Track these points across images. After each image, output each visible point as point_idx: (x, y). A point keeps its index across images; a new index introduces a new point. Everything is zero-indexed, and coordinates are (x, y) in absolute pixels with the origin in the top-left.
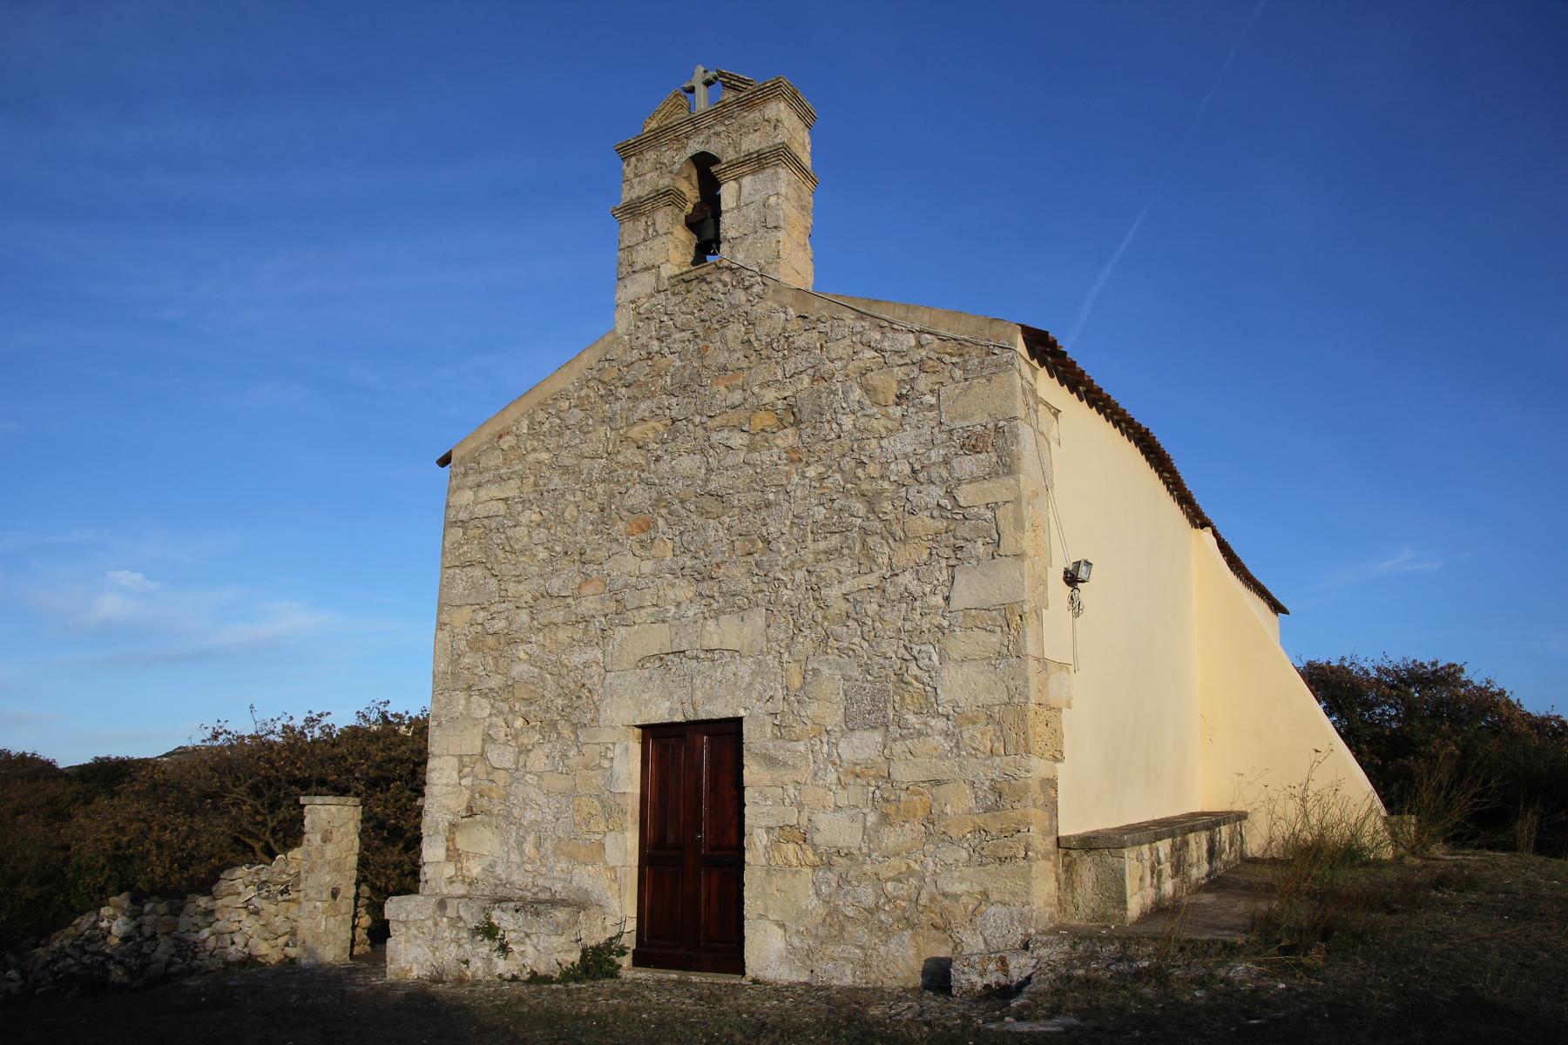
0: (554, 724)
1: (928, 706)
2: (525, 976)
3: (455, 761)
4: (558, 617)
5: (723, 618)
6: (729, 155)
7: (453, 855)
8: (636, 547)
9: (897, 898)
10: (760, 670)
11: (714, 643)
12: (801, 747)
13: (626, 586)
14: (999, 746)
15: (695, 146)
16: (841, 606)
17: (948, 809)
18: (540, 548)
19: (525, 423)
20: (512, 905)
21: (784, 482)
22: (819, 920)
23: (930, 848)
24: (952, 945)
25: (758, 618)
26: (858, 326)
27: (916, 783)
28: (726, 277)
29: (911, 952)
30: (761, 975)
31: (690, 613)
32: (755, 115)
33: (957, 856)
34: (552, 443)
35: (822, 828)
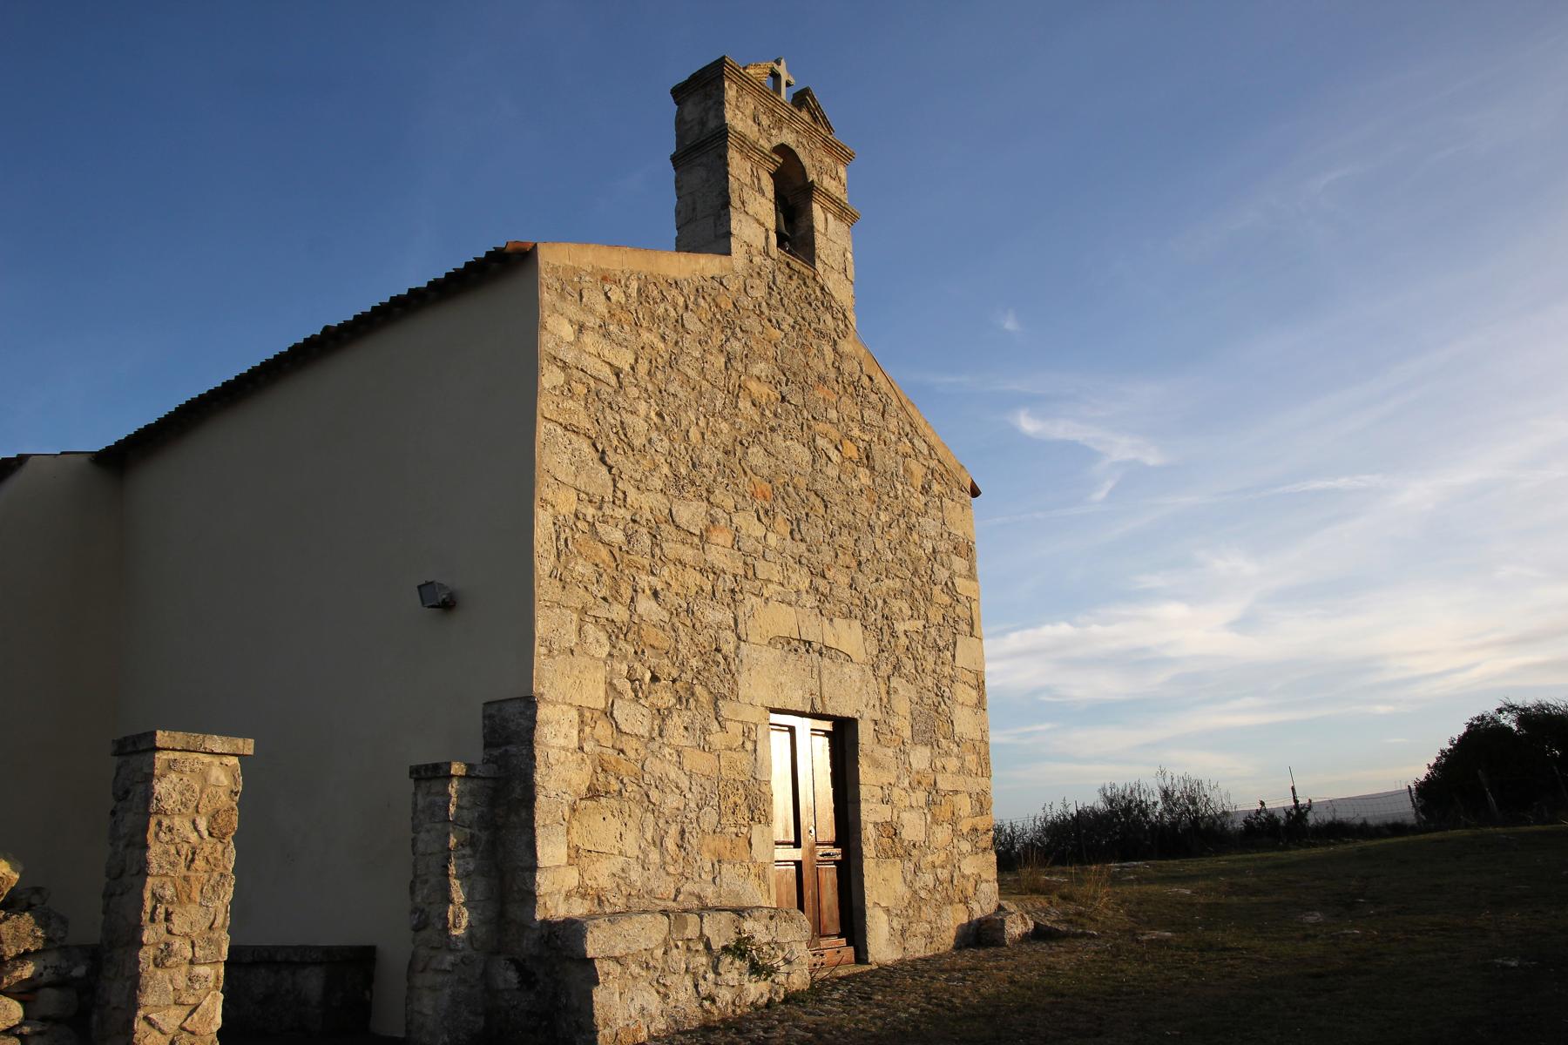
1: (951, 736)
3: (574, 714)
4: (689, 554)
12: (890, 752)
15: (788, 138)
19: (634, 285)
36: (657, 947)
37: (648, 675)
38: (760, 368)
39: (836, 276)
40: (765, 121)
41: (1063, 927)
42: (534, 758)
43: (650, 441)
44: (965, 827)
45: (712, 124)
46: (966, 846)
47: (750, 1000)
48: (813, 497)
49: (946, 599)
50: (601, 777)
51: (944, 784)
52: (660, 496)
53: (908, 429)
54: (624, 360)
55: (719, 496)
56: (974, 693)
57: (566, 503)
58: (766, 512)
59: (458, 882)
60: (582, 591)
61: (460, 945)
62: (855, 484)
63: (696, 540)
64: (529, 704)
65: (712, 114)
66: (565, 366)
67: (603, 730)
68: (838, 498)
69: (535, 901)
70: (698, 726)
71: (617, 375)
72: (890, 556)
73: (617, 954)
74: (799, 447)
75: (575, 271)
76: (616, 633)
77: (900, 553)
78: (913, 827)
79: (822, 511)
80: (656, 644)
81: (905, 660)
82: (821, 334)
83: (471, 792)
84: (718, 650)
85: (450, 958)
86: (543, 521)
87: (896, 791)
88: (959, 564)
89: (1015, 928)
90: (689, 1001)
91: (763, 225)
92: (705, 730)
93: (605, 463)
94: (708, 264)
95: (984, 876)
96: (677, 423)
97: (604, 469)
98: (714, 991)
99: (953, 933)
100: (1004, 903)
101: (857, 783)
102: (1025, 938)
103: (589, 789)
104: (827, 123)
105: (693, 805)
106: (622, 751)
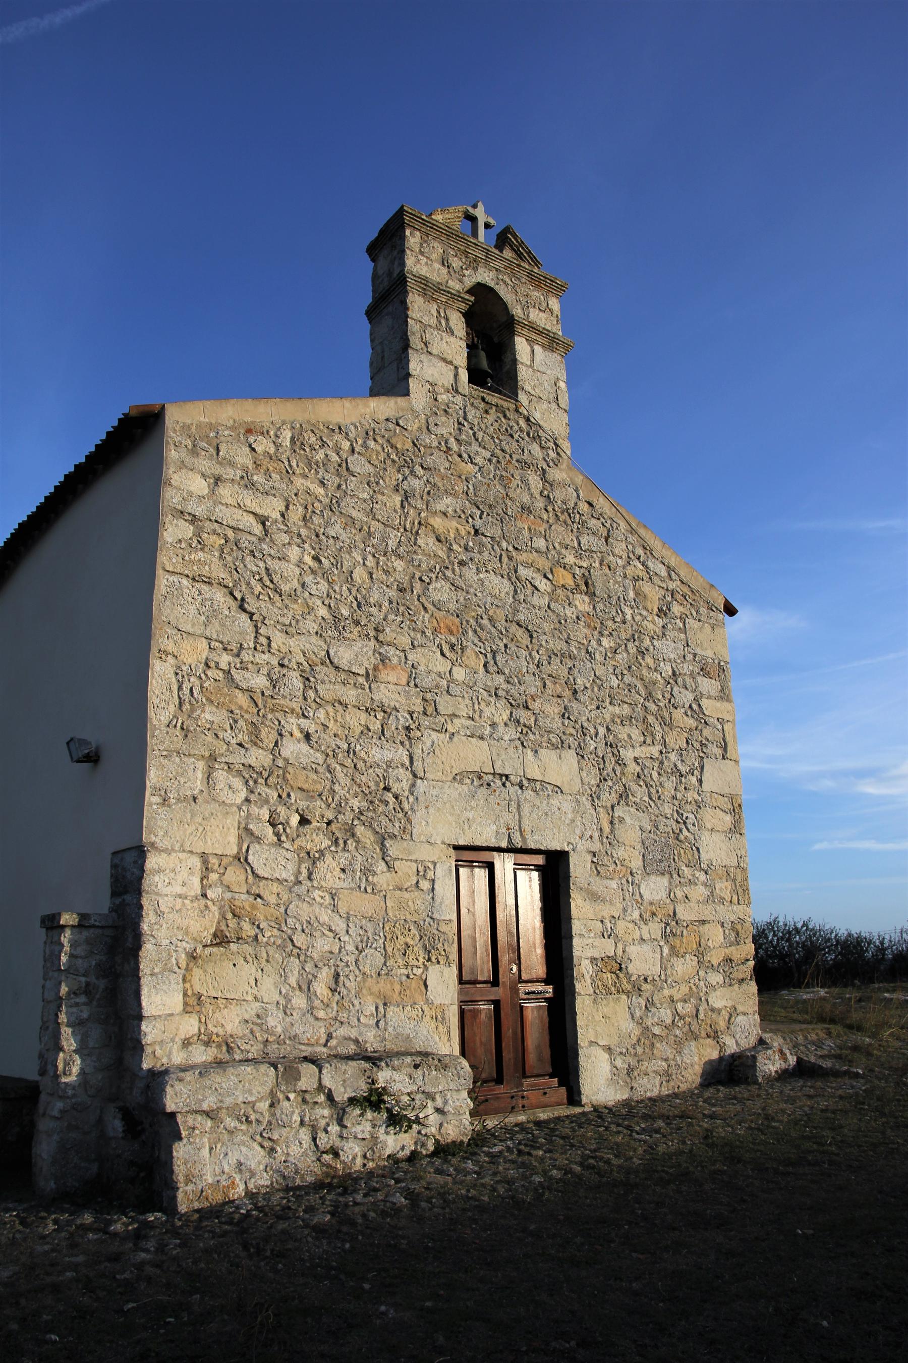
1: (695, 864)
3: (196, 862)
4: (350, 695)
7: (194, 1003)
12: (614, 884)
13: (437, 687)
15: (485, 276)
16: (633, 768)
17: (710, 944)
19: (287, 434)
20: (408, 1060)
36: (260, 1100)
37: (295, 819)
38: (446, 503)
39: (545, 406)
40: (456, 263)
41: (827, 1064)
42: (141, 907)
43: (303, 585)
44: (715, 958)
45: (397, 271)
46: (716, 978)
47: (388, 1152)
48: (514, 628)
49: (692, 723)
50: (232, 923)
51: (685, 913)
52: (314, 639)
53: (640, 551)
54: (272, 508)
55: (389, 634)
56: (728, 818)
57: (194, 653)
58: (452, 647)
59: (69, 1030)
60: (210, 738)
61: (70, 1092)
62: (569, 612)
63: (361, 680)
64: (140, 852)
65: (396, 263)
66: (194, 519)
67: (235, 876)
68: (547, 627)
69: (143, 1050)
70: (358, 867)
71: (263, 524)
72: (615, 682)
73: (205, 1107)
74: (496, 580)
75: (211, 427)
76: (252, 777)
77: (628, 679)
78: (643, 960)
79: (526, 640)
80: (306, 787)
81: (634, 787)
82: (525, 465)
83: (88, 941)
84: (387, 789)
85: (60, 1105)
86: (160, 675)
87: (621, 925)
88: (707, 685)
89: (770, 1065)
90: (305, 1154)
91: (451, 363)
92: (367, 871)
93: (245, 610)
94: (384, 407)
95: (740, 1008)
96: (337, 563)
97: (244, 617)
98: (338, 1143)
99: (698, 1069)
100: (767, 1036)
101: (569, 918)
102: (784, 1075)
103: (215, 935)
104: (533, 258)
105: (350, 948)
106: (259, 896)
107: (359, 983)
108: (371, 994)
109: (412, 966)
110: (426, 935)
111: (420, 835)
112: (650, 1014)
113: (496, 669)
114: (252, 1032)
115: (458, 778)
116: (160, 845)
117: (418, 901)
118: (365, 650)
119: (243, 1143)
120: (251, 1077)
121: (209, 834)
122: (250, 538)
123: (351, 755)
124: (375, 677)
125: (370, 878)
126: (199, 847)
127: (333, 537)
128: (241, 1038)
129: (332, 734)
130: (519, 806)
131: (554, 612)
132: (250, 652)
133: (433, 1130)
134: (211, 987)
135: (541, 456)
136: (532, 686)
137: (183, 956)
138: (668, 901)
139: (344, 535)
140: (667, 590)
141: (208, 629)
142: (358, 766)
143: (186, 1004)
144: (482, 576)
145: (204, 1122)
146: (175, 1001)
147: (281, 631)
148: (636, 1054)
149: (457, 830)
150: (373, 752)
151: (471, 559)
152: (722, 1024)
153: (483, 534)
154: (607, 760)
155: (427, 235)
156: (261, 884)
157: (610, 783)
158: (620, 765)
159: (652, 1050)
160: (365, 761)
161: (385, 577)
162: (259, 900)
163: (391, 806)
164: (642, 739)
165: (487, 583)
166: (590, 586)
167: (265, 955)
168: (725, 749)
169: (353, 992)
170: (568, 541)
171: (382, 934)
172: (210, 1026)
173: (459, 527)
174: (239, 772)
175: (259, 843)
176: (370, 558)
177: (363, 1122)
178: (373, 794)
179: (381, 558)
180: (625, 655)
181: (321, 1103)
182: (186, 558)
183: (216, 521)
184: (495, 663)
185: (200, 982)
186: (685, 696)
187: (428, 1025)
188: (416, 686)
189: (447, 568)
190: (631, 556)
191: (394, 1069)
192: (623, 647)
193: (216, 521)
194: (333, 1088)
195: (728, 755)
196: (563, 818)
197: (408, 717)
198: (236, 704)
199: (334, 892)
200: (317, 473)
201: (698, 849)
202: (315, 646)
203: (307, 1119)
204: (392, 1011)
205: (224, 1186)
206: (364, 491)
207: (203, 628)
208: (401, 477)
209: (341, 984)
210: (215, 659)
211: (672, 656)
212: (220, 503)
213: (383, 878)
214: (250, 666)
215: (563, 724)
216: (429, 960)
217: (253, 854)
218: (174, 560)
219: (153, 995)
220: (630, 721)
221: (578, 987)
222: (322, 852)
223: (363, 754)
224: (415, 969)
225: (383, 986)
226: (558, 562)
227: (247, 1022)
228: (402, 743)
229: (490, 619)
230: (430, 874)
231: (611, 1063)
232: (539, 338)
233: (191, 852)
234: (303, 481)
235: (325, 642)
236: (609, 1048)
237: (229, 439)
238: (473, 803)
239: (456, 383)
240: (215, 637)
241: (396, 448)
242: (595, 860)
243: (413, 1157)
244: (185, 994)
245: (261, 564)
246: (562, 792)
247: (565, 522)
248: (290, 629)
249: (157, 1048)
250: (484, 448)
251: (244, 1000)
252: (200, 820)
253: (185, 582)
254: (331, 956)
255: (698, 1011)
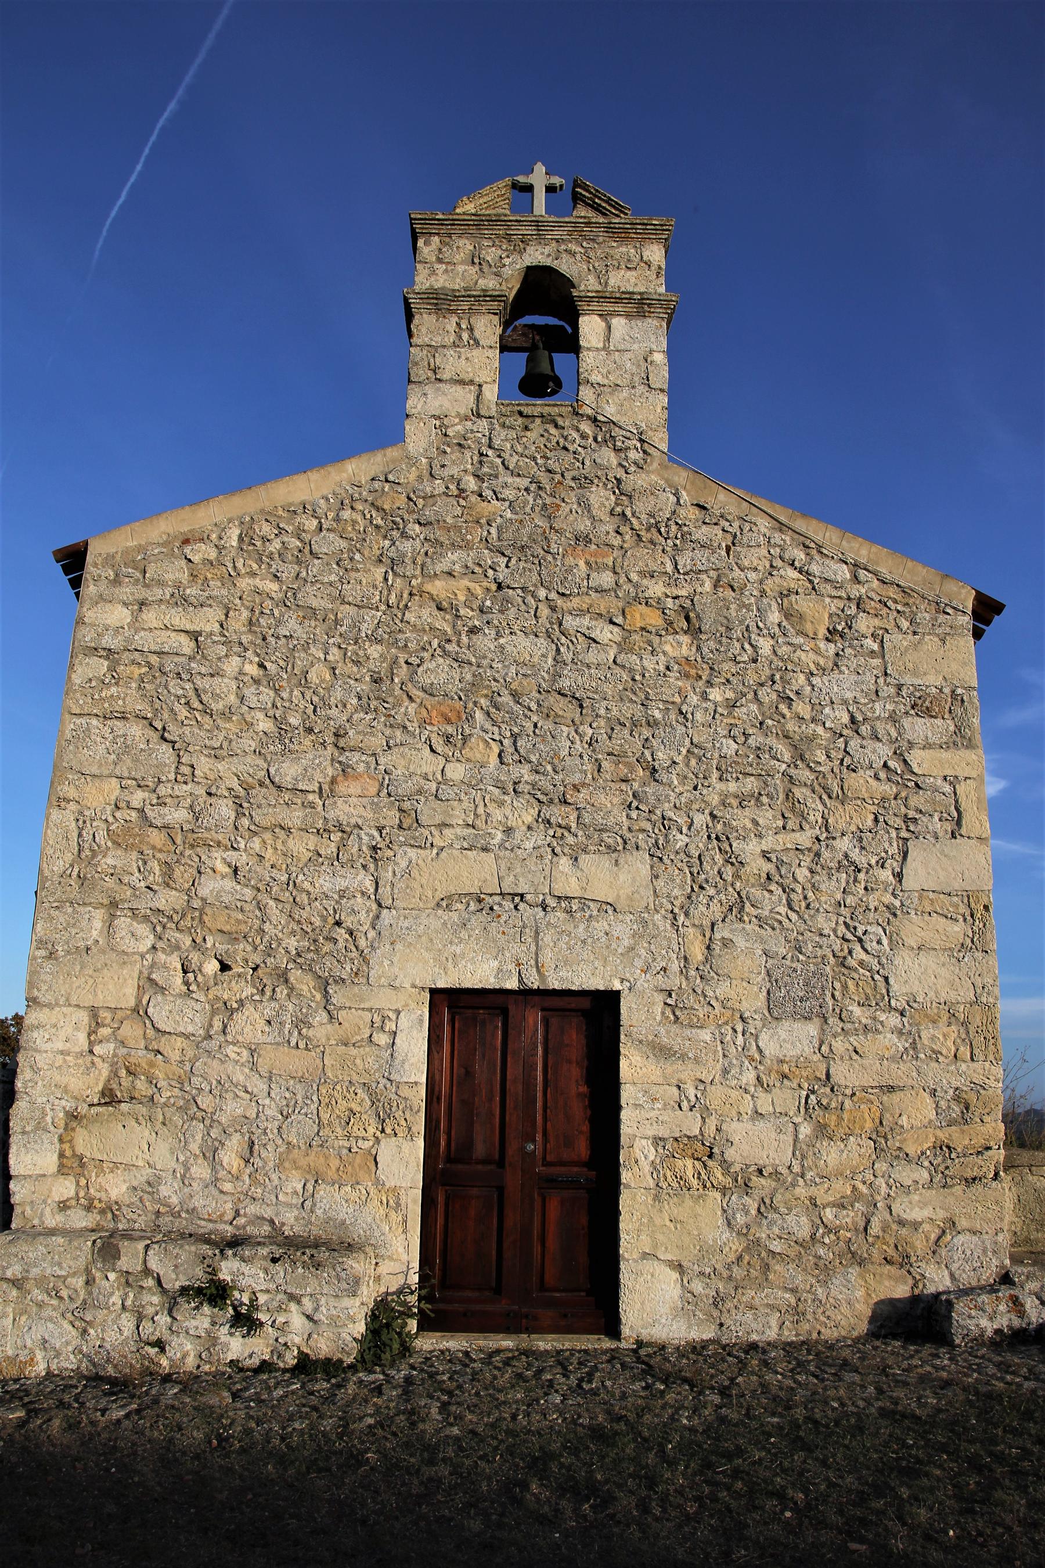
0: (283, 977)
1: (880, 996)
2: (290, 1359)
3: (84, 1017)
4: (295, 817)
5: (583, 858)
6: (587, 284)
7: (72, 1164)
8: (438, 744)
9: (841, 1227)
10: (643, 929)
11: (571, 887)
12: (706, 1035)
13: (420, 792)
14: (965, 1051)
15: (537, 255)
16: (758, 866)
17: (904, 1121)
18: (260, 715)
19: (234, 533)
21: (677, 699)
22: (732, 1257)
23: (881, 1166)
24: (911, 1282)
25: (639, 865)
26: (777, 538)
27: (864, 1089)
28: (586, 427)
29: (860, 1293)
30: (645, 1334)
31: (529, 845)
32: (628, 250)
33: (915, 1176)
34: (288, 571)
35: (736, 1139)
40: (491, 254)
48: (552, 699)
54: (208, 621)
58: (448, 739)
67: (131, 1031)
73: (9, 1274)
92: (301, 1023)
97: (165, 747)
98: (166, 1336)
103: (103, 1094)
107: (281, 1154)
108: (297, 1168)
109: (357, 1138)
110: (379, 1100)
111: (380, 978)
112: (765, 1222)
113: (516, 757)
114: (141, 1199)
115: (445, 903)
116: (42, 999)
117: (367, 1060)
118: (317, 761)
119: (51, 1319)
120: (62, 1249)
121: (100, 986)
122: (176, 659)
123: (291, 887)
124: (331, 791)
125: (304, 1031)
126: (88, 1001)
127: (285, 636)
128: (128, 1206)
129: (268, 865)
130: (537, 933)
131: (623, 667)
132: (169, 785)
133: (297, 1340)
134: (95, 1149)
135: (614, 462)
136: (580, 770)
137: (61, 1115)
138: (817, 1057)
139: (300, 631)
140: (849, 599)
141: (118, 767)
142: (298, 899)
143: (61, 1166)
144: (502, 641)
145: (8, 1291)
146: (49, 1161)
147: (209, 756)
148: (730, 1278)
149: (437, 969)
150: (321, 881)
151: (488, 623)
152: (920, 1244)
153: (508, 587)
154: (706, 859)
155: (450, 236)
156: (163, 1039)
157: (712, 892)
158: (732, 864)
159: (765, 1274)
160: (309, 893)
161: (355, 669)
162: (159, 1056)
163: (341, 944)
164: (780, 823)
165: (509, 648)
166: (694, 620)
167: (161, 1117)
168: (959, 823)
169: (271, 1164)
170: (653, 566)
171: (315, 1098)
172: (92, 1191)
173: (471, 585)
174: (146, 918)
175: (164, 994)
176: (335, 650)
177: (198, 1317)
178: (318, 931)
179: (350, 648)
180: (754, 707)
181: (150, 1289)
182: (96, 697)
183: (136, 650)
184: (516, 750)
185: (84, 1142)
186: (874, 751)
187: (375, 1210)
188: (389, 795)
189: (449, 641)
190: (778, 563)
191: (243, 1260)
192: (750, 696)
193: (136, 650)
194: (161, 1274)
195: (963, 831)
196: (614, 946)
197: (376, 834)
198: (148, 843)
199: (253, 1047)
200: (270, 566)
201: (886, 979)
202: (251, 766)
203: (129, 1302)
204: (323, 1190)
205: (21, 1362)
206: (331, 573)
207: (112, 767)
208: (387, 543)
209: (255, 1155)
210: (126, 799)
211: (849, 695)
212: (143, 629)
213: (320, 1029)
214: (168, 800)
215: (628, 817)
216: (383, 1131)
217: (155, 1006)
218: (81, 702)
219: (22, 1154)
220: (757, 799)
221: (625, 1176)
222: (241, 1003)
223: (306, 885)
224: (360, 1142)
225: (314, 1159)
226: (636, 598)
227: (135, 1188)
228: (364, 867)
229: (515, 695)
230: (390, 1026)
231: (682, 1286)
232: (619, 308)
233: (78, 1006)
234: (250, 581)
235: (265, 760)
236: (680, 1265)
237: (161, 556)
238: (464, 934)
239: (477, 406)
240: (126, 774)
241: (383, 510)
242: (669, 1001)
243: (265, 1366)
244: (62, 1155)
245: (188, 686)
246: (615, 910)
247: (652, 542)
248: (219, 752)
249: (28, 1209)
250: (519, 475)
251: (133, 1165)
252: (91, 972)
253: (94, 722)
254: (246, 1121)
255: (868, 1222)
